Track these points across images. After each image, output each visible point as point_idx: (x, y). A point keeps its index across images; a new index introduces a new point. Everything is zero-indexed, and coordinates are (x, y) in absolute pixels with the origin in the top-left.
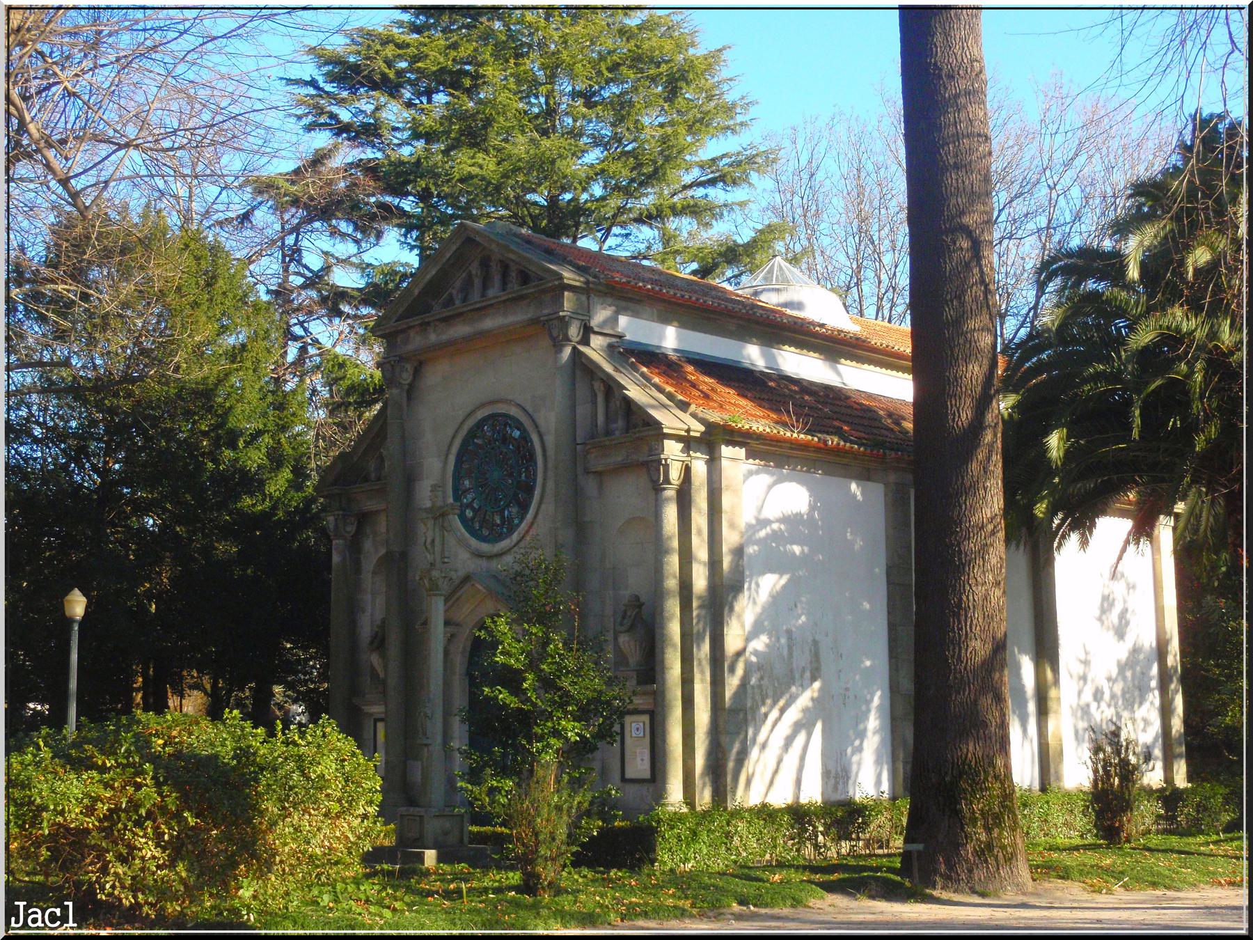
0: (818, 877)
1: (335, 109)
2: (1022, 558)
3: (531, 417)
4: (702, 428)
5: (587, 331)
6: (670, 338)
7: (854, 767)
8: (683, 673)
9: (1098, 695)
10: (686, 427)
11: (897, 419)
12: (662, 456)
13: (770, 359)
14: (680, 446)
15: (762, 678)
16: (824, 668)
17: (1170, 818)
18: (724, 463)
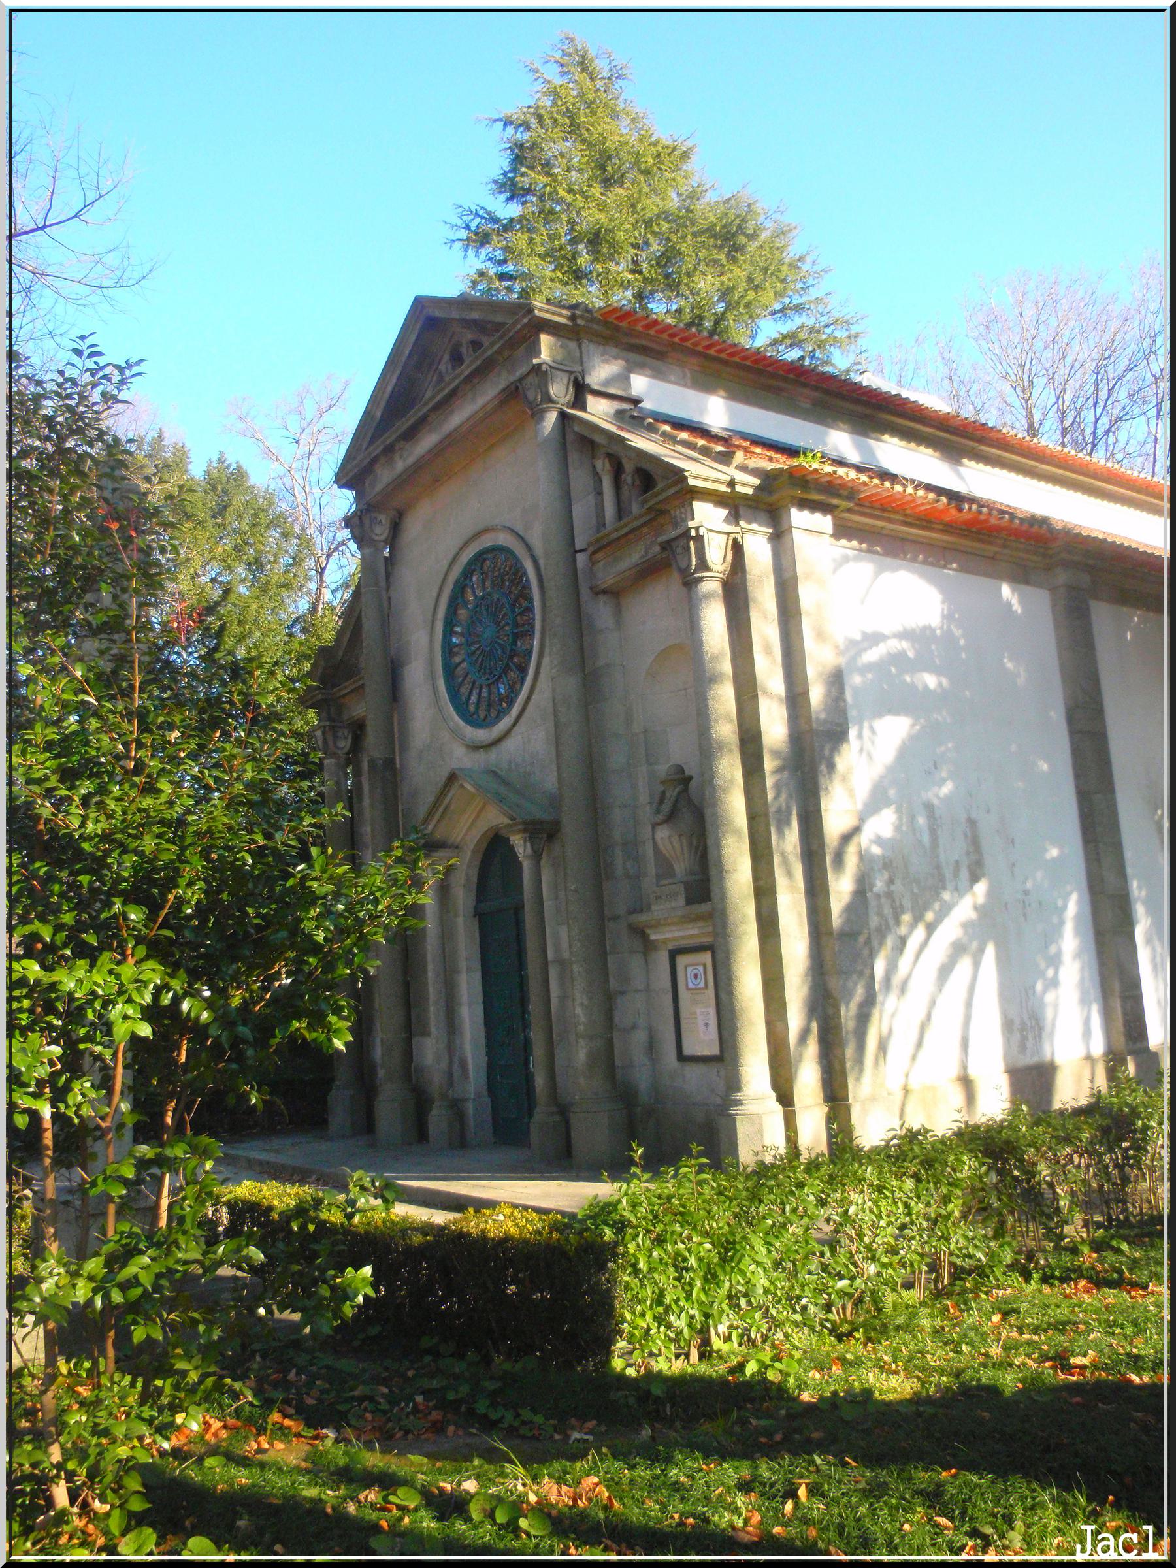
3: (522, 539)
4: (756, 482)
5: (581, 390)
7: (1049, 1013)
8: (756, 879)
10: (728, 479)
12: (691, 524)
14: (723, 512)
15: (891, 881)
16: (988, 861)
18: (798, 537)
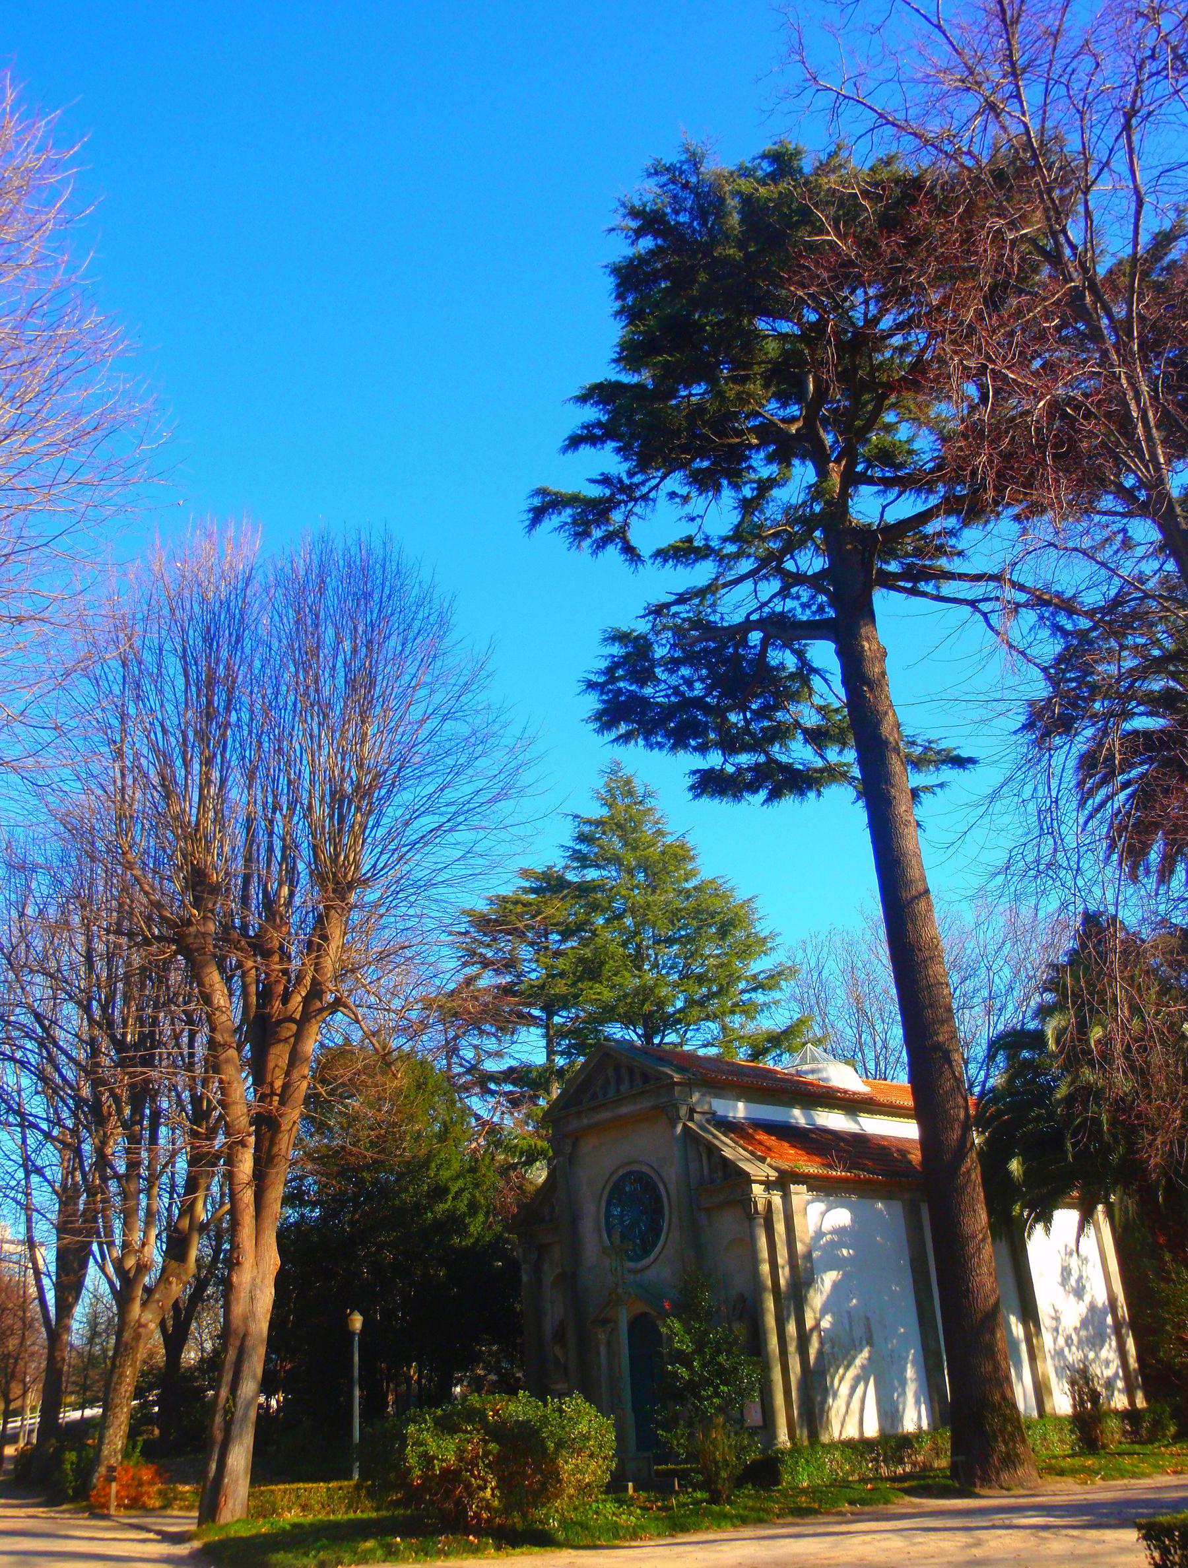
0: (896, 1485)
1: (483, 951)
2: (1004, 1246)
6: (740, 1110)
9: (1068, 1339)
11: (904, 1153)
13: (809, 1118)
14: (763, 1187)
17: (1135, 1432)
